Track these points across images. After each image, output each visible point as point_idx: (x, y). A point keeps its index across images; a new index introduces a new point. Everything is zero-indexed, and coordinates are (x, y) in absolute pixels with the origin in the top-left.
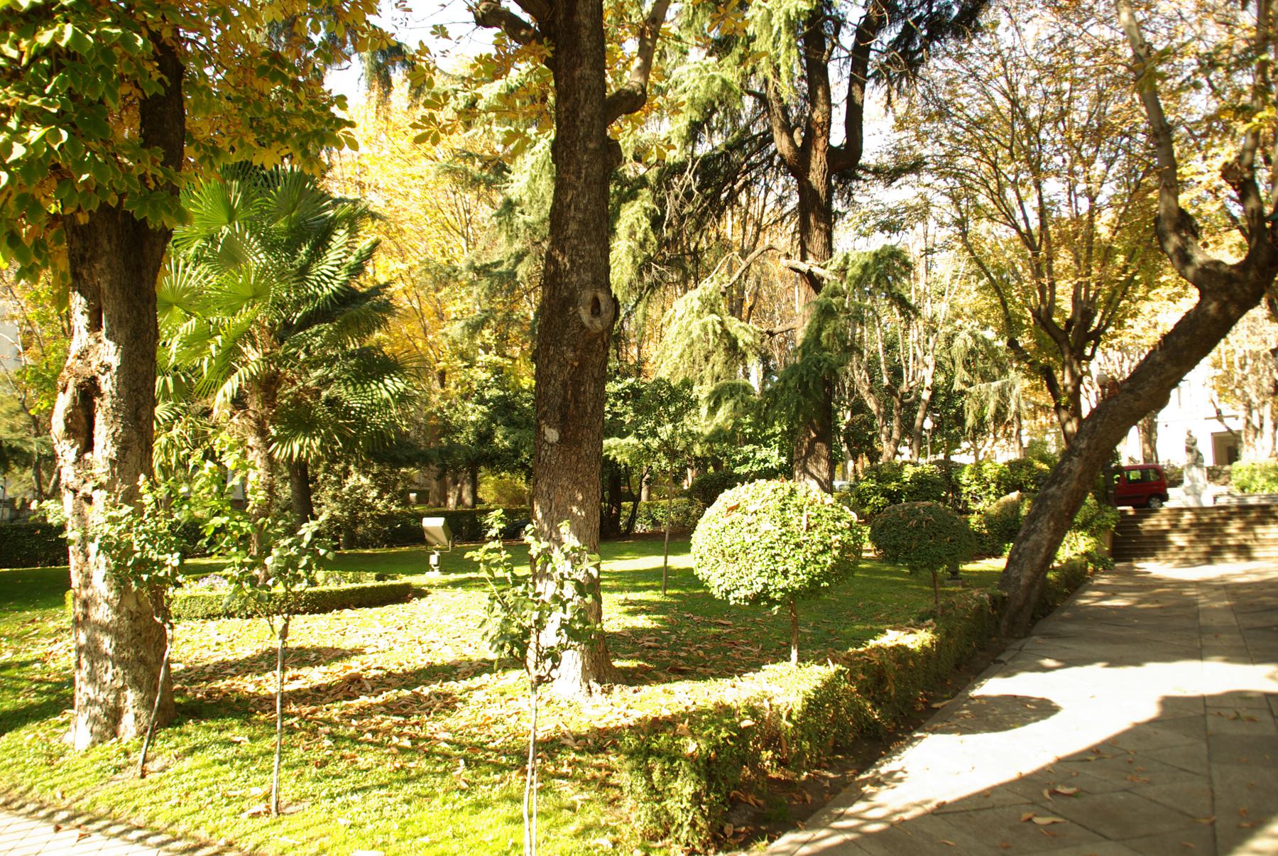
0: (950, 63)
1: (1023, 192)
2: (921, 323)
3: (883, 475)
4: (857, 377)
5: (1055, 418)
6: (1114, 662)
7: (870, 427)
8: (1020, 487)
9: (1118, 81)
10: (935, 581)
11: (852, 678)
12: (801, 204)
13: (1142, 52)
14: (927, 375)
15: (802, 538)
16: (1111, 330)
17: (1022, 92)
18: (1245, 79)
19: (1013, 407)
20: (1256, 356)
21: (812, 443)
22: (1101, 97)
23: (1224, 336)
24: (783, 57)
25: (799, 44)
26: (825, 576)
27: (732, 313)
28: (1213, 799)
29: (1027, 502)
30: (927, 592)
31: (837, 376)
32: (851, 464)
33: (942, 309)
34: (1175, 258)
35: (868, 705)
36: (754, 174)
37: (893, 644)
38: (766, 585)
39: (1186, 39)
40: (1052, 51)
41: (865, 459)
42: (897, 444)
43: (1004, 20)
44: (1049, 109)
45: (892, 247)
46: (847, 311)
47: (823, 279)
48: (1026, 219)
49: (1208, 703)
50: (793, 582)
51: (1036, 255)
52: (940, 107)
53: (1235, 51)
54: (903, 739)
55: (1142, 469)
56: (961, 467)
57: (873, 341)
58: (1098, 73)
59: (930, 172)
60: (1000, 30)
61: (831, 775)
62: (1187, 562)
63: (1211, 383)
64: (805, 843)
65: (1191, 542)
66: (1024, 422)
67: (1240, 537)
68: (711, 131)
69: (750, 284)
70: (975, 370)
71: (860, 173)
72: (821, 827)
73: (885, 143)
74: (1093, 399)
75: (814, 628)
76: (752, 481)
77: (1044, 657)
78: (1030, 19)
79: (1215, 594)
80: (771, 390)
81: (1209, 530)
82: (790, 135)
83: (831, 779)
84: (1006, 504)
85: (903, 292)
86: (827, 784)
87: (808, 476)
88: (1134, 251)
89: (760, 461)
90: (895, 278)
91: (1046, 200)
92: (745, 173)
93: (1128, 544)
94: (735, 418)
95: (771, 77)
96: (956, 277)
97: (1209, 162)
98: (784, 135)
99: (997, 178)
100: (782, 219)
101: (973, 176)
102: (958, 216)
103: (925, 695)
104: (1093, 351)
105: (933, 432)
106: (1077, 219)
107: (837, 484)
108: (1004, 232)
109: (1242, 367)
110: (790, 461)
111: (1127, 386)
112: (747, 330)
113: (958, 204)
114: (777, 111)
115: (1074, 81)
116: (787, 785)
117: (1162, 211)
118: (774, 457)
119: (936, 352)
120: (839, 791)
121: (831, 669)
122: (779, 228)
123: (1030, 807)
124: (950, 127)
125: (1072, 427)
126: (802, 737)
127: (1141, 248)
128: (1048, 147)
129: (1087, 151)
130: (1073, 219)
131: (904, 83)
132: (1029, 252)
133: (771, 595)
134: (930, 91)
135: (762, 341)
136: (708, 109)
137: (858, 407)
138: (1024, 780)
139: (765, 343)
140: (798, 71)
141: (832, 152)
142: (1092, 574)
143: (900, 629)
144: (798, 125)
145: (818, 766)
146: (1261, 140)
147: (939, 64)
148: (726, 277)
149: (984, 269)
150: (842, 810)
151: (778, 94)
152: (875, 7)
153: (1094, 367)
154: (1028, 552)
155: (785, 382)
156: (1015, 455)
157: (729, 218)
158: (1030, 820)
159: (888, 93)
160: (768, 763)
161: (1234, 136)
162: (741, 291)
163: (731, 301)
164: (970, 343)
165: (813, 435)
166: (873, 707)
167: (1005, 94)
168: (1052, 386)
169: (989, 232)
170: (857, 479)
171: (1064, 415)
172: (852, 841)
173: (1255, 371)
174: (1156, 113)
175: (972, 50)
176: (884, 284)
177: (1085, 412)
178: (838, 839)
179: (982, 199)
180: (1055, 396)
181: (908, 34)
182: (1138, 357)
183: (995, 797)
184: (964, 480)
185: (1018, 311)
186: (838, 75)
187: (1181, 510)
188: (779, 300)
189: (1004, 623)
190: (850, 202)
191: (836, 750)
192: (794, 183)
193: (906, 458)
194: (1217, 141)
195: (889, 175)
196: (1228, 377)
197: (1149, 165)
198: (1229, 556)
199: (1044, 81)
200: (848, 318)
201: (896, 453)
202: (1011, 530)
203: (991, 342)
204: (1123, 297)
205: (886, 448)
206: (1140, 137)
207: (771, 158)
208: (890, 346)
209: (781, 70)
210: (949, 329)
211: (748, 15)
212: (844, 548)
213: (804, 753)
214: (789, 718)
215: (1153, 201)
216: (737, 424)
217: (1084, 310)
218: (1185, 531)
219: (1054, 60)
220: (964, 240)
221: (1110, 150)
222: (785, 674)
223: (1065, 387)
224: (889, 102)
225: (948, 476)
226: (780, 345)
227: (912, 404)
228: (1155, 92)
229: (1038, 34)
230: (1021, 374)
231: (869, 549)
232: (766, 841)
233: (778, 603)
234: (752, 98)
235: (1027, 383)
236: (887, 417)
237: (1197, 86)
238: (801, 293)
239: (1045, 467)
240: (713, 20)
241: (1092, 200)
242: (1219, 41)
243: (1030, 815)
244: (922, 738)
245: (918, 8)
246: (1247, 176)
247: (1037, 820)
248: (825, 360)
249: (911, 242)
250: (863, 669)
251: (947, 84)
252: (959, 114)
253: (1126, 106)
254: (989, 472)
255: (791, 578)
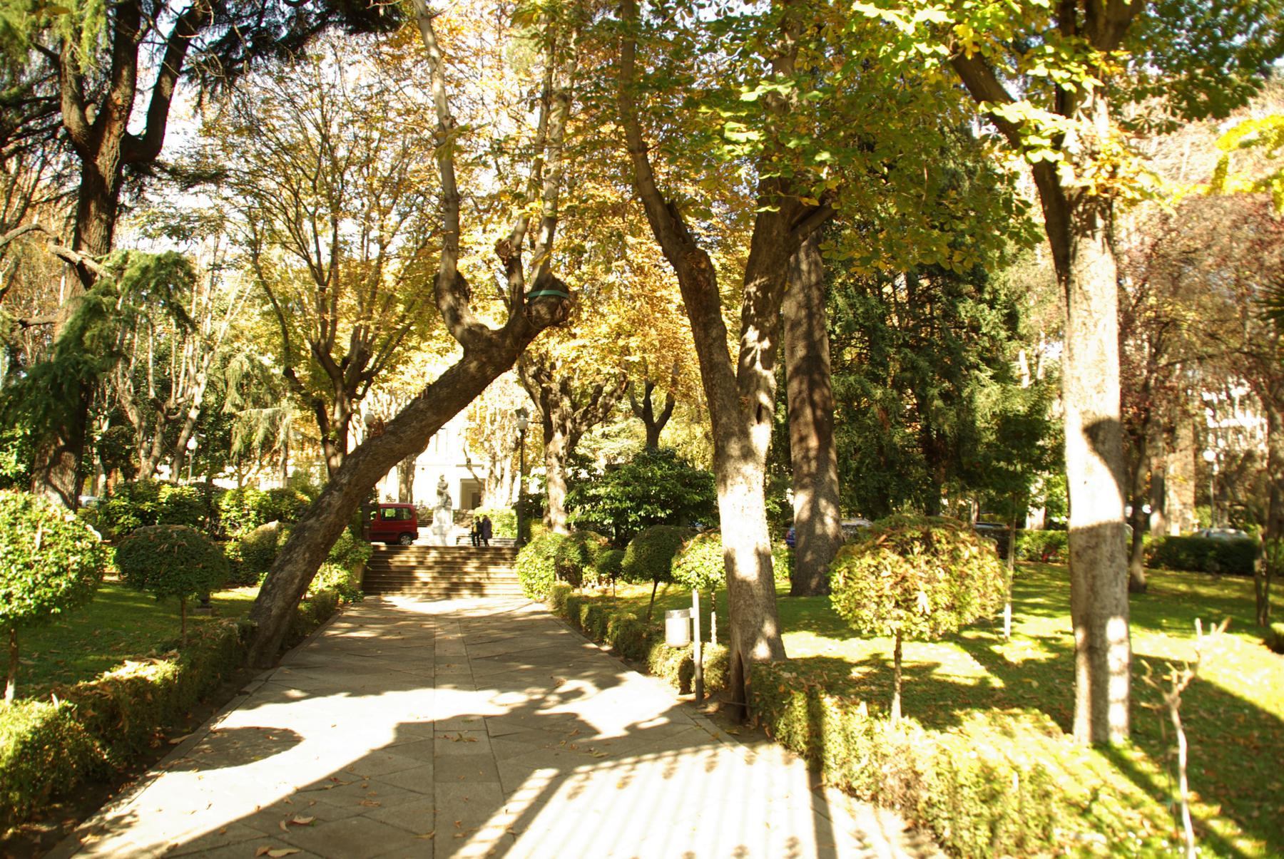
0: (270, 82)
1: (319, 226)
2: (197, 338)
3: (139, 493)
4: (121, 386)
5: (322, 451)
6: (356, 692)
7: (129, 441)
8: (280, 517)
9: (420, 142)
10: (183, 609)
11: (80, 715)
12: (81, 188)
13: (447, 123)
14: (197, 393)
15: (32, 558)
16: (383, 373)
17: (334, 129)
18: (524, 171)
19: (282, 437)
21: (59, 451)
22: (405, 153)
23: (480, 393)
25: (110, 13)
26: (58, 601)
28: (435, 815)
29: (285, 532)
30: (174, 621)
31: (97, 382)
32: (102, 478)
33: (222, 328)
34: (447, 316)
35: (97, 744)
36: (30, 141)
37: (131, 676)
40: (369, 98)
41: (119, 474)
42: (156, 462)
43: (329, 57)
44: (357, 152)
46: (118, 313)
47: (95, 274)
49: (437, 727)
51: (323, 290)
52: (251, 122)
54: (135, 779)
55: (398, 508)
57: (143, 349)
58: (406, 131)
59: (231, 185)
60: (323, 65)
61: (44, 828)
62: (429, 597)
63: (464, 434)
65: (434, 578)
66: (291, 453)
67: (477, 575)
70: (248, 395)
71: (156, 169)
73: (188, 145)
75: (39, 658)
77: (290, 688)
78: (354, 63)
79: (450, 627)
80: (16, 388)
81: (449, 567)
82: (82, 109)
84: (264, 532)
85: (183, 303)
87: (49, 488)
90: (176, 287)
91: (340, 238)
92: (19, 137)
93: (379, 578)
95: (69, 39)
96: (241, 297)
97: (487, 235)
98: (75, 107)
100: (58, 199)
101: (273, 199)
102: (252, 236)
103: (163, 731)
104: (365, 391)
105: (198, 453)
107: (83, 499)
109: (492, 422)
110: (30, 469)
111: (390, 428)
113: (254, 225)
114: (70, 78)
115: (383, 132)
117: (441, 271)
119: (210, 371)
120: (53, 846)
123: (266, 841)
124: (258, 146)
127: (420, 301)
128: (351, 188)
130: (362, 262)
131: (219, 88)
132: (317, 286)
135: (12, 330)
137: (118, 418)
138: (262, 814)
139: (16, 333)
140: (103, 42)
141: (127, 140)
142: (342, 606)
143: (140, 660)
144: (92, 101)
145: (28, 820)
146: (529, 227)
147: (258, 80)
149: (270, 294)
151: (75, 61)
153: (364, 406)
154: (281, 582)
155: (35, 380)
156: (278, 484)
158: (265, 853)
159: (201, 95)
161: (510, 217)
164: (247, 366)
165: (62, 443)
167: (317, 127)
170: (107, 495)
171: (330, 450)
174: (450, 181)
175: (293, 76)
176: (163, 291)
177: (351, 448)
179: (279, 225)
180: (324, 430)
181: (231, 41)
182: (404, 403)
184: (224, 505)
186: (149, 61)
187: (428, 548)
188: (40, 287)
190: (139, 198)
191: (53, 798)
192: (77, 162)
193: (165, 477)
194: (495, 218)
195: (188, 179)
196: (479, 430)
197: (437, 227)
198: (465, 592)
199: (357, 125)
200: (119, 321)
201: (155, 471)
202: (267, 560)
203: (267, 369)
204: (398, 344)
205: (144, 465)
206: (433, 199)
207: (55, 128)
208: (162, 358)
209: (83, 35)
210: (226, 349)
212: (83, 570)
213: (11, 807)
215: (436, 261)
217: (361, 349)
218: (430, 568)
219: (369, 109)
220: (255, 262)
221: (406, 204)
223: (334, 422)
224: (200, 104)
225: (208, 499)
226: (34, 338)
227: (177, 421)
228: (452, 162)
230: (293, 404)
231: (112, 572)
235: (298, 414)
238: (66, 286)
239: (306, 498)
241: (383, 247)
243: (266, 849)
244: (156, 777)
245: (248, 17)
246: (515, 254)
248: (85, 362)
249: (199, 252)
251: (263, 102)
253: (423, 165)
254: (251, 500)
255: (15, 603)
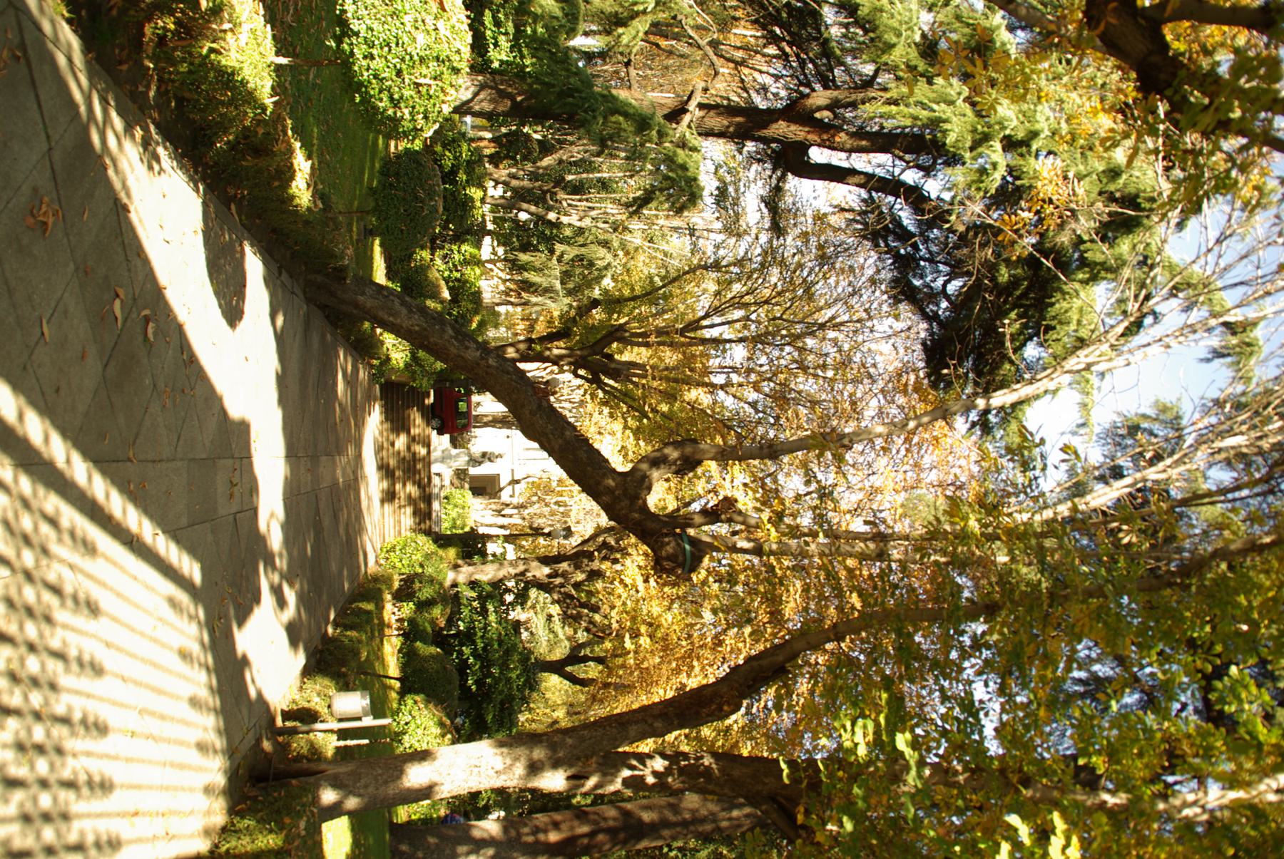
0: (869, 272)
1: (738, 325)
2: (624, 217)
4: (576, 149)
5: (522, 338)
6: (281, 380)
7: (525, 158)
8: (455, 300)
9: (825, 419)
10: (362, 212)
11: (259, 122)
12: (756, 109)
13: (846, 442)
14: (573, 219)
15: (407, 77)
16: (601, 394)
17: (831, 334)
18: (806, 521)
19: (534, 299)
20: (566, 514)
21: (511, 97)
22: (814, 403)
24: (906, 110)
26: (366, 99)
27: (655, 25)
29: (439, 307)
30: (351, 204)
32: (488, 135)
33: (636, 239)
34: (657, 454)
36: (794, 64)
38: (357, 34)
39: (850, 477)
40: (864, 365)
42: (505, 183)
43: (899, 326)
44: (810, 358)
45: (701, 196)
46: (642, 145)
47: (678, 123)
48: (712, 326)
49: (245, 461)
50: (360, 63)
52: (830, 257)
53: (830, 514)
54: (196, 172)
56: (478, 245)
57: (609, 168)
58: (836, 403)
59: (770, 241)
60: (891, 320)
61: (152, 94)
62: (379, 449)
63: (544, 476)
64: (70, 60)
65: (399, 453)
66: (519, 309)
68: (846, 26)
69: (682, 47)
71: (779, 173)
72: (90, 79)
74: (537, 374)
75: (315, 85)
76: (471, 27)
77: (285, 316)
78: (896, 349)
79: (349, 471)
81: (408, 469)
82: (827, 108)
83: (147, 93)
84: (438, 286)
86: (141, 89)
88: (671, 420)
89: (495, 38)
90: (670, 196)
91: (728, 346)
92: (797, 56)
93: (397, 398)
94: (542, 17)
96: (666, 255)
97: (741, 488)
98: (828, 102)
99: (755, 303)
100: (745, 89)
102: (724, 263)
105: (515, 221)
106: (707, 372)
107: (468, 119)
108: (705, 303)
109: (557, 503)
110: (494, 72)
111: (545, 404)
112: (634, 38)
113: (735, 265)
114: (853, 97)
116: (137, 42)
117: (702, 446)
118: (500, 54)
119: (594, 230)
120: (135, 102)
121: (269, 102)
122: (735, 85)
124: (810, 264)
125: (511, 353)
126: (191, 64)
127: (672, 425)
128: (776, 353)
129: (767, 387)
131: (860, 226)
133: (346, 40)
134: (846, 250)
135: (622, 54)
136: (868, 25)
140: (889, 124)
141: (803, 147)
142: (369, 363)
143: (312, 174)
144: (836, 116)
147: (871, 261)
148: (692, 23)
149: (670, 283)
150: (112, 103)
152: (935, 208)
153: (568, 376)
154: (390, 304)
155: (576, 74)
156: (487, 297)
157: (753, 33)
158: (118, 296)
159: (851, 210)
160: (160, 23)
162: (677, 37)
163: (668, 25)
164: (600, 264)
165: (519, 99)
166: (228, 142)
167: (833, 318)
168: (551, 337)
169: (705, 291)
170: (472, 140)
171: (522, 346)
172: (78, 113)
173: (553, 514)
174: (791, 448)
175: (878, 293)
176: (665, 184)
178: (78, 96)
179: (737, 287)
180: (542, 340)
181: (904, 235)
183: (139, 263)
184: (465, 247)
185: (626, 310)
187: (429, 446)
188: (663, 76)
189: (319, 278)
190: (752, 159)
191: (180, 101)
192: (779, 105)
193: (491, 192)
198: (385, 484)
199: (838, 355)
201: (497, 183)
203: (599, 283)
205: (503, 173)
207: (808, 85)
210: (616, 244)
211: (954, 81)
212: (396, 121)
213: (173, 65)
214: (212, 50)
216: (536, 18)
217: (622, 371)
218: (409, 448)
220: (700, 267)
221: (766, 407)
222: (262, 49)
223: (549, 349)
224: (843, 210)
227: (545, 201)
229: (881, 354)
232: (67, 15)
233: (338, 47)
234: (871, 73)
235: (556, 314)
236: (534, 176)
237: (808, 483)
239: (474, 325)
240: (956, 42)
242: (842, 502)
243: (122, 296)
244: (197, 191)
245: (927, 248)
247: (118, 302)
248: (595, 117)
249: (705, 216)
250: (268, 134)
252: (821, 275)
253: (800, 423)
254: (471, 273)
255: (364, 63)
